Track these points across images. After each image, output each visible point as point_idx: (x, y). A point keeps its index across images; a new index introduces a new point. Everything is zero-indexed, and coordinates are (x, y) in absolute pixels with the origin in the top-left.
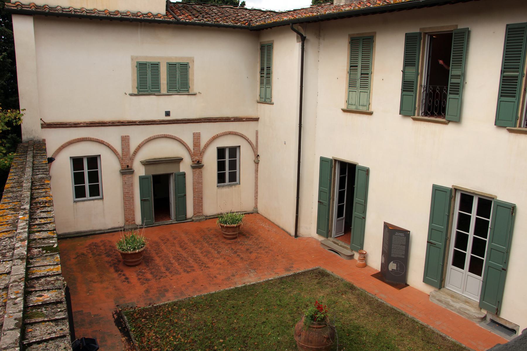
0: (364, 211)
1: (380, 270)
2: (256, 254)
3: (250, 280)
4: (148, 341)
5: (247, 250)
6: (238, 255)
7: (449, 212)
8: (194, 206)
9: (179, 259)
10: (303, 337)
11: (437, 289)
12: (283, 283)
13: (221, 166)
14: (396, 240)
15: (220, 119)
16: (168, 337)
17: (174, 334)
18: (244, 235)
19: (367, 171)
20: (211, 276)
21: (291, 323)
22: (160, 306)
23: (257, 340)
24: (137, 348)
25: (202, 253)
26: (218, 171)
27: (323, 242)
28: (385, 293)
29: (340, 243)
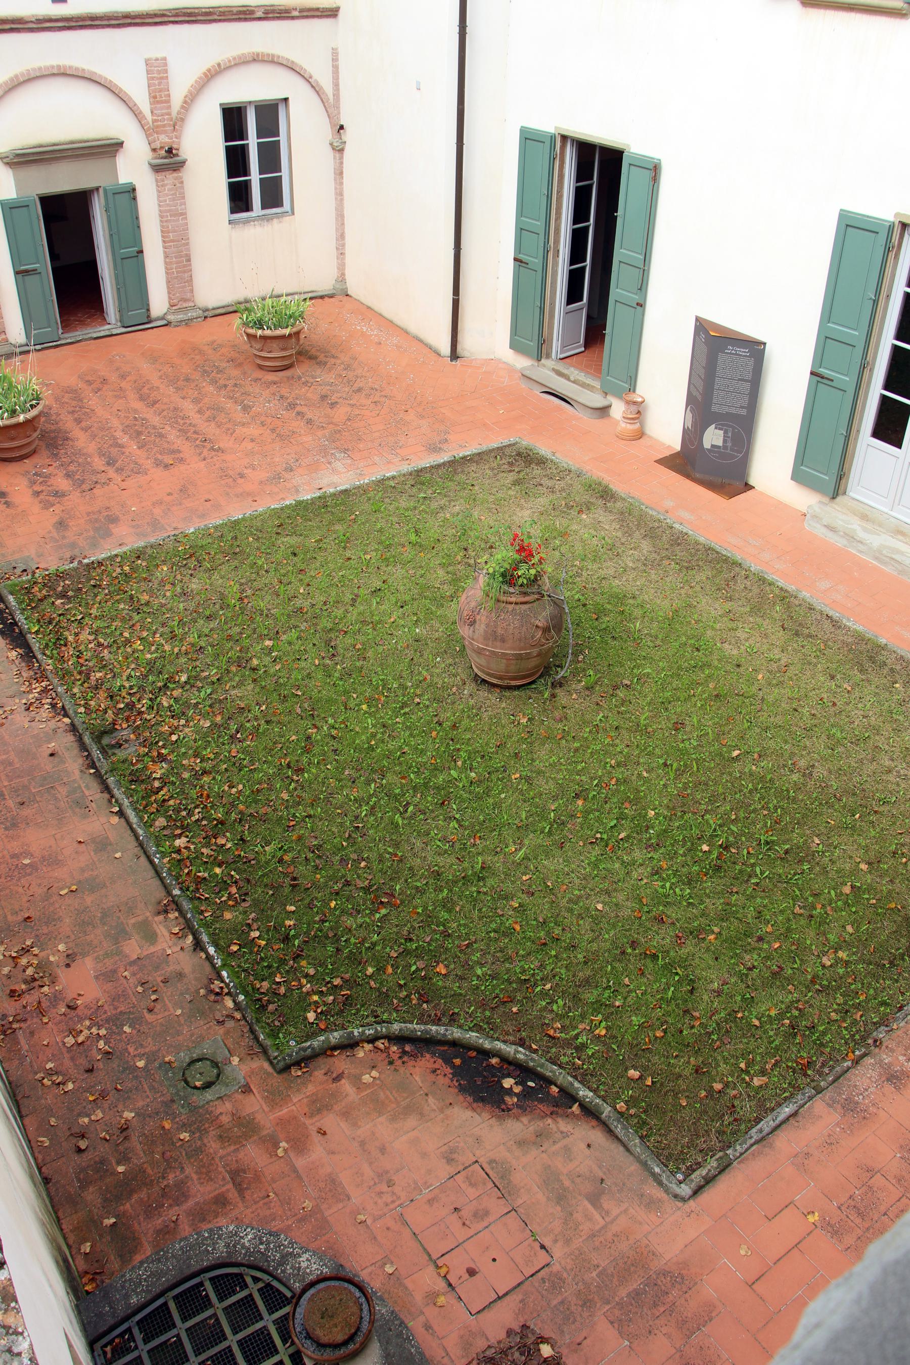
0: (642, 287)
1: (678, 447)
2: (349, 409)
3: (335, 479)
4: (78, 657)
5: (324, 397)
6: (298, 413)
7: (878, 292)
8: (168, 282)
9: (139, 433)
10: (481, 628)
11: (826, 500)
12: (423, 484)
13: (236, 161)
14: (727, 364)
15: (222, 14)
16: (128, 642)
17: (145, 634)
18: (312, 358)
19: (655, 170)
20: (231, 473)
21: (448, 590)
22: (100, 564)
23: (361, 638)
24: (50, 676)
25: (200, 412)
26: (230, 176)
27: (527, 373)
28: (692, 509)
29: (574, 373)
